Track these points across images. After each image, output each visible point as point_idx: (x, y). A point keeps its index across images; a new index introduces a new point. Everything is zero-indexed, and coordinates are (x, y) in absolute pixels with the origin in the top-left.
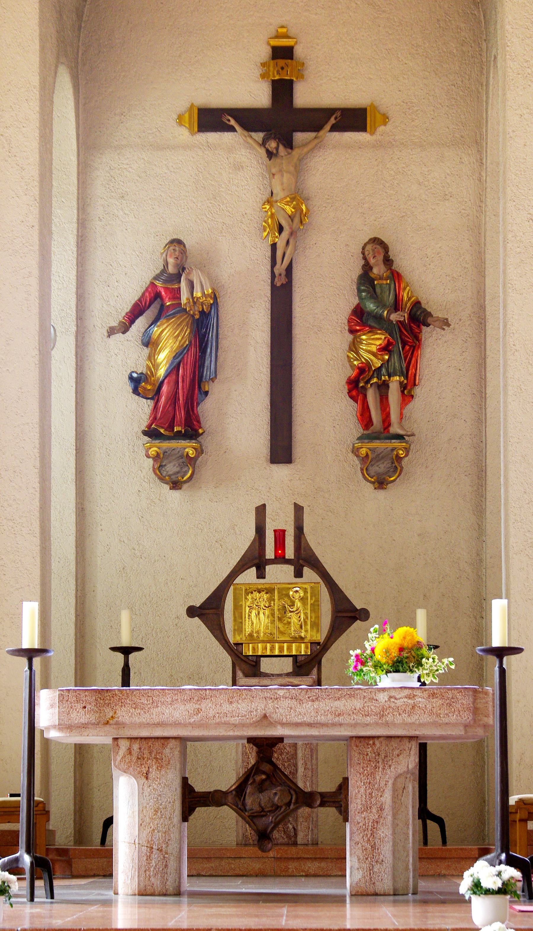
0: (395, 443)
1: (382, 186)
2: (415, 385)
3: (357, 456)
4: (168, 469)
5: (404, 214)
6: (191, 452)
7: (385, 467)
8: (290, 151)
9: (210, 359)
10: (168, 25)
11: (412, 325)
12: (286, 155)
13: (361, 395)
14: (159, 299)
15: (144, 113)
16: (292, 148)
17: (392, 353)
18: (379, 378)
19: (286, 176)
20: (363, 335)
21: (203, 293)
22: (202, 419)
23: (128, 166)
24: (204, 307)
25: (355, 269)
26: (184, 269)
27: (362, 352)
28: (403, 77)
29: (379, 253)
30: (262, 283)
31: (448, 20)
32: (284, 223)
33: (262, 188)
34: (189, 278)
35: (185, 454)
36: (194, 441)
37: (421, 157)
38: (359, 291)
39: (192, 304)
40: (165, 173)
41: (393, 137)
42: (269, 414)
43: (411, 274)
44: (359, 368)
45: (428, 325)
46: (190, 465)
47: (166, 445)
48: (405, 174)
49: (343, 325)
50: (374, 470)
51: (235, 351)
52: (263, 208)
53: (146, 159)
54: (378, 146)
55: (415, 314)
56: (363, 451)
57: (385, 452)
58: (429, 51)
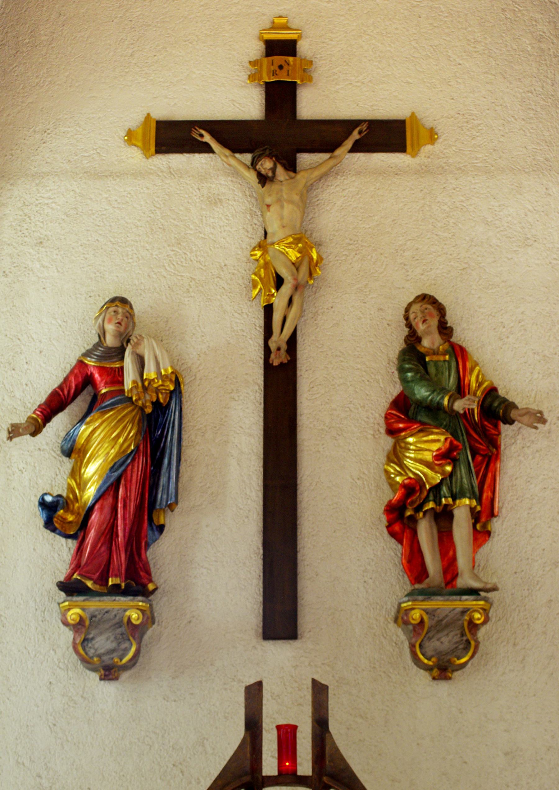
0: (468, 602)
1: (430, 226)
2: (492, 515)
3: (406, 623)
4: (96, 646)
5: (466, 266)
6: (135, 616)
7: (449, 642)
8: (292, 174)
9: (167, 475)
10: (116, 17)
11: (486, 423)
12: (287, 180)
13: (408, 531)
14: (89, 388)
15: (77, 130)
16: (295, 171)
17: (458, 463)
18: (437, 501)
19: (288, 209)
20: (411, 436)
21: (159, 372)
22: (153, 570)
23: (51, 201)
24: (160, 396)
25: (396, 342)
26: (128, 341)
27: (408, 463)
28: (457, 81)
29: (431, 315)
30: (250, 364)
31: (517, 10)
32: (284, 273)
33: (250, 229)
34: (138, 351)
35: (125, 620)
36: (140, 598)
37: (488, 187)
38: (402, 370)
39: (140, 389)
40: (106, 210)
41: (445, 160)
42: (261, 562)
43: (480, 351)
44: (403, 486)
45: (511, 422)
46: (134, 638)
47: (95, 604)
48: (465, 210)
49: (376, 426)
50: (433, 645)
51: (207, 466)
52: (252, 255)
53: (78, 191)
54: (423, 171)
55: (491, 405)
56: (416, 615)
57: (451, 615)
58: (492, 48)
